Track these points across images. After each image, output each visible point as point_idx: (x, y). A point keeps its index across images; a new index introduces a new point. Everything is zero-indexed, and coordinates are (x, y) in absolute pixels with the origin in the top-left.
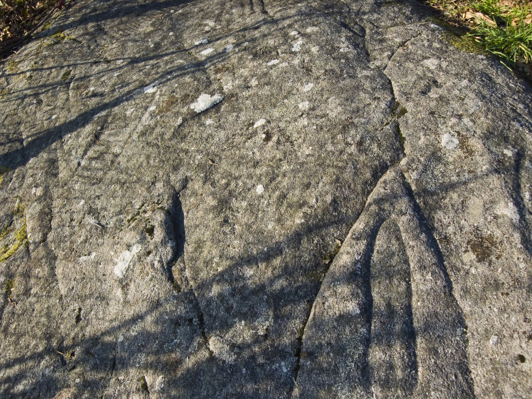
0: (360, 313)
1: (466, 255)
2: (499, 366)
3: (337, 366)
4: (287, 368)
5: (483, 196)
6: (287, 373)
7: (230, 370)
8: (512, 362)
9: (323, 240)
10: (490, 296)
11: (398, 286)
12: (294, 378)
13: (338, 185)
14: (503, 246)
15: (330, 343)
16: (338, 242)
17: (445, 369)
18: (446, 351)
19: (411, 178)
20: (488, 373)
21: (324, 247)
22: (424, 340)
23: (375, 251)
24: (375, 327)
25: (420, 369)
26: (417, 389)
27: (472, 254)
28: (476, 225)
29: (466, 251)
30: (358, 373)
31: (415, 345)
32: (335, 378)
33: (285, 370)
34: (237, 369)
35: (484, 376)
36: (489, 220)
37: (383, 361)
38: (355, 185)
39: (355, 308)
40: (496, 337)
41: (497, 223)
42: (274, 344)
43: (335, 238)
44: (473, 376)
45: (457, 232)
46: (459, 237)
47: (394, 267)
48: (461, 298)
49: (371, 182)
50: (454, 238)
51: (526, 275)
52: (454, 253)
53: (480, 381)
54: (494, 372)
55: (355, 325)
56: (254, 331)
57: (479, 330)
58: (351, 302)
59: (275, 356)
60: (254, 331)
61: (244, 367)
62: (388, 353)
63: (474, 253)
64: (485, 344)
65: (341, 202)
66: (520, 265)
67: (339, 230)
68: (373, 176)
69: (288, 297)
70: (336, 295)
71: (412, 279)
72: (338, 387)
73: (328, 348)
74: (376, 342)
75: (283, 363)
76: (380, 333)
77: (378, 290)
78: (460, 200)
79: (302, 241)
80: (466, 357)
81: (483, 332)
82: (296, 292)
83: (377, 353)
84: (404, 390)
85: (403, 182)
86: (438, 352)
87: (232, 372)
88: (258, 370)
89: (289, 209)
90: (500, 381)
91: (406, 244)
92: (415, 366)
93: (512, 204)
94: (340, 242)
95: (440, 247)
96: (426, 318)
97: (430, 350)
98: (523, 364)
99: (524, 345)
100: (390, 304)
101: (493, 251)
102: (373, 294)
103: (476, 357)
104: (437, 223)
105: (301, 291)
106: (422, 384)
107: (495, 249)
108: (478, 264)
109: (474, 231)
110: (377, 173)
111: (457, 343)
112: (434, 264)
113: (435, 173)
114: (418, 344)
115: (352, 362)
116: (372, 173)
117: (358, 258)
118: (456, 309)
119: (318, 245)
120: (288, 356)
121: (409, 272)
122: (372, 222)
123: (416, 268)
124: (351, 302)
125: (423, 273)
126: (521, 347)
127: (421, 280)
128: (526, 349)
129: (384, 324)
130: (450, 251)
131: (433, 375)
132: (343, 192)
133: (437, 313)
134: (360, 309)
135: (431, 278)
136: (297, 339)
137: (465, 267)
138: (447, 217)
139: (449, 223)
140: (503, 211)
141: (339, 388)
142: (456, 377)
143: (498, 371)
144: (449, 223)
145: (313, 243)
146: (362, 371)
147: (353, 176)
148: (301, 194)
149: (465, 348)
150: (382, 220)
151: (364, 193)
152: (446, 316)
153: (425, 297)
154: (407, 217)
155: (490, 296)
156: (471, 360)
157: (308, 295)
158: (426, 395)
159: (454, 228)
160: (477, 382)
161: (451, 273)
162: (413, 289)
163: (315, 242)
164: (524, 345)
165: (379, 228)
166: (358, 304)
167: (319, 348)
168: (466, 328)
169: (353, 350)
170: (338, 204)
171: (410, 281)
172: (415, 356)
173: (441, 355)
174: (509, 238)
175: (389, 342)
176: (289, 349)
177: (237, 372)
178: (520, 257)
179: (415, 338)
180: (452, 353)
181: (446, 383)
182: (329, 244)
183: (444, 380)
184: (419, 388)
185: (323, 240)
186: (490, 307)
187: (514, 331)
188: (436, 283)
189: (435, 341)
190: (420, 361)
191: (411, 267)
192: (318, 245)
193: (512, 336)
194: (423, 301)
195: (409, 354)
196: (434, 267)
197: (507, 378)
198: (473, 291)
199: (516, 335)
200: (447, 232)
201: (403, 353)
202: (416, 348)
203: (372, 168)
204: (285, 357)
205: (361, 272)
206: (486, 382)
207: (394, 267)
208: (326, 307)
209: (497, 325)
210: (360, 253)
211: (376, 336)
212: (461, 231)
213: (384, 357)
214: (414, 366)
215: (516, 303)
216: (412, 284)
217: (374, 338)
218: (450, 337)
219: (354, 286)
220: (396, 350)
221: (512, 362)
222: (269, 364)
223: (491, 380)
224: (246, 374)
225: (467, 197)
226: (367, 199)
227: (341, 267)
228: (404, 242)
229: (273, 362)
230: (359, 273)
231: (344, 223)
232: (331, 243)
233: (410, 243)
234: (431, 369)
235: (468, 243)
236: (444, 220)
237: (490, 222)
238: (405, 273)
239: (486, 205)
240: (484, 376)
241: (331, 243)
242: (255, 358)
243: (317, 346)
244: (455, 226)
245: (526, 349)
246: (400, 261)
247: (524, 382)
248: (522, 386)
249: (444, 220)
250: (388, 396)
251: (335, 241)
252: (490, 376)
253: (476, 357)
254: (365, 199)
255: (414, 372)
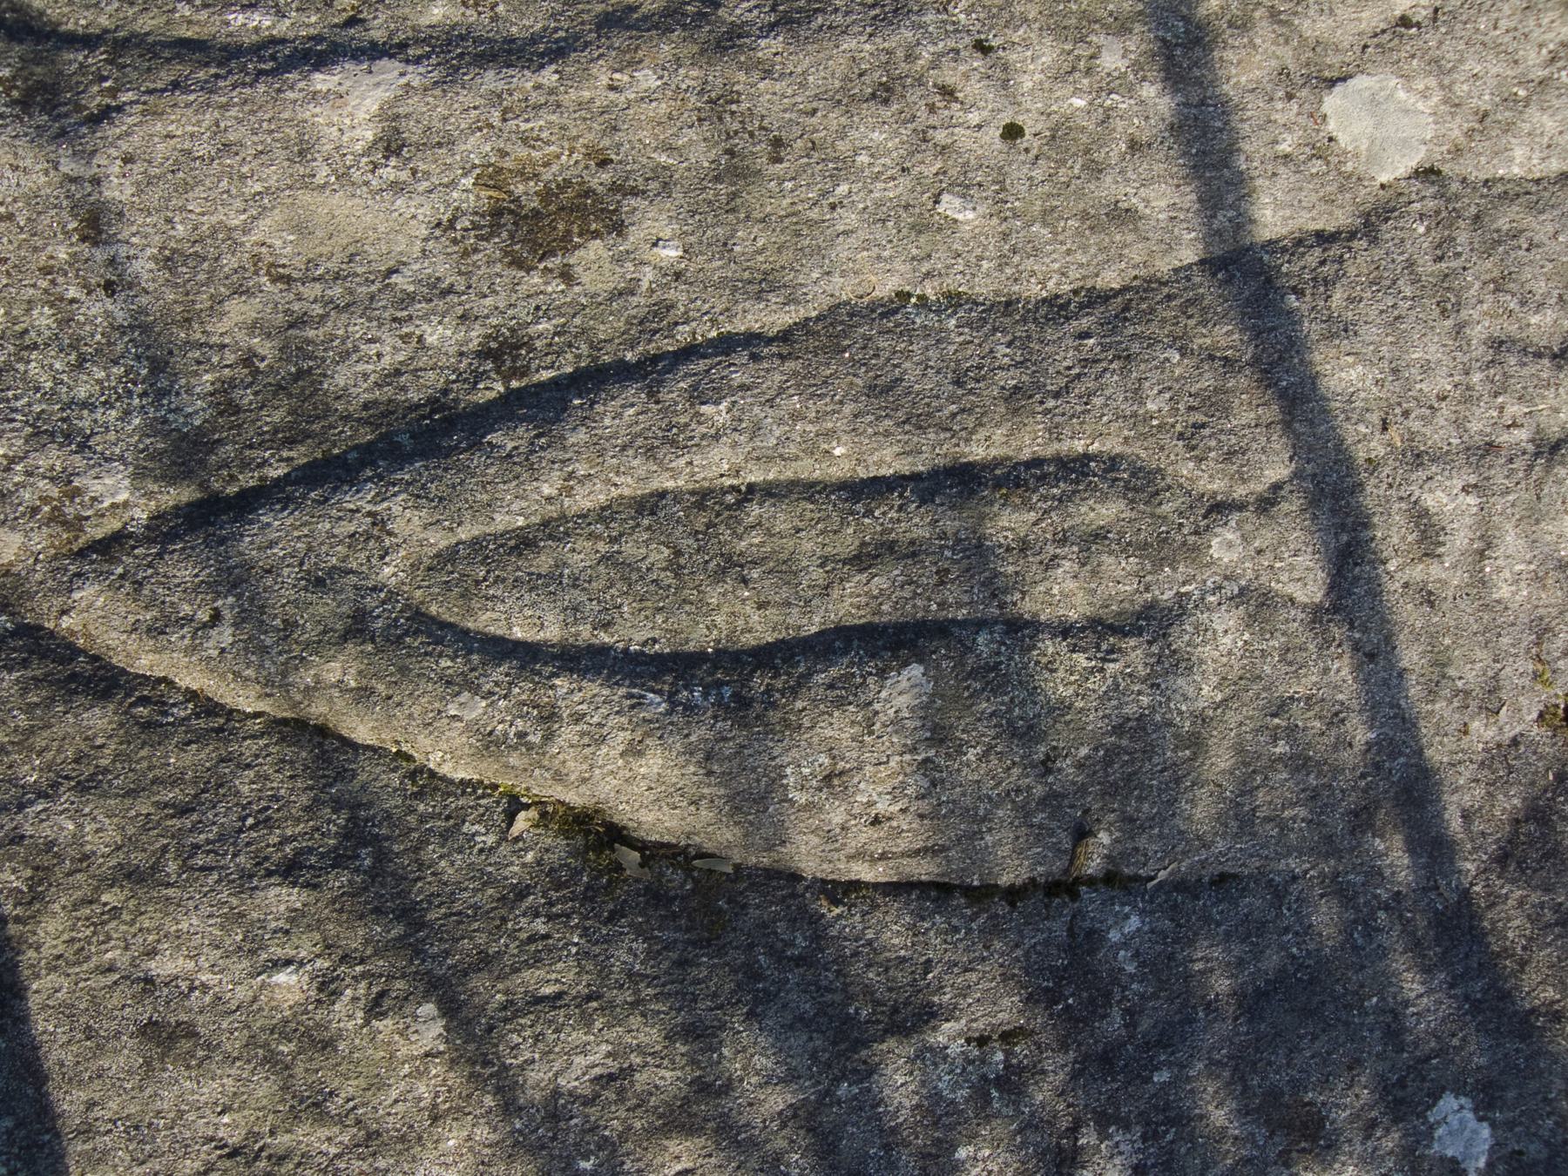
0: (920, 662)
1: (586, 278)
2: (1039, 203)
3: (1121, 726)
4: (1127, 917)
5: (258, 187)
6: (1142, 912)
7: (1166, 1132)
8: (1024, 163)
9: (522, 893)
10: (786, 202)
11: (769, 533)
12: (1150, 885)
13: (172, 867)
14: (544, 135)
15: (1043, 763)
16: (522, 822)
17: (1069, 368)
18: (1006, 360)
19: (126, 504)
20: (1060, 238)
21: (559, 886)
22: (982, 434)
23: (605, 638)
24: (960, 605)
25: (1079, 446)
26: (1143, 454)
27: (580, 253)
28: (425, 232)
29: (567, 275)
30: (1134, 649)
31: (998, 462)
32: (1158, 728)
33: (1134, 922)
34: (1156, 1107)
35: (1069, 252)
36: (404, 175)
37: (1084, 565)
38: (175, 781)
39: (904, 684)
40: (945, 198)
41: (420, 147)
42: (1047, 990)
43: (503, 838)
44: (1067, 288)
45: (459, 311)
46: (488, 301)
47: (678, 553)
48: (796, 302)
49: (144, 701)
50: (494, 321)
51: (694, 73)
52: (577, 321)
53: (1081, 265)
54: (1058, 220)
55: (969, 675)
56: (995, 1094)
57: (914, 251)
58: (877, 706)
59: (1094, 973)
60: (995, 1094)
61: (1149, 1080)
62: (1051, 550)
63: (577, 247)
64: (967, 236)
65: (285, 840)
66: (644, 86)
67: (457, 826)
68: (104, 695)
69: (828, 990)
70: (842, 773)
71: (728, 482)
72: (1180, 713)
73: (1060, 770)
74: (1017, 596)
75: (1114, 936)
76: (983, 584)
77: (795, 611)
78: (268, 287)
79: (548, 990)
80: (1008, 304)
81: (922, 239)
82: (799, 961)
83: (1055, 591)
84: (1157, 493)
85: (150, 541)
86: (1015, 387)
87: (1170, 1122)
88: (1145, 1024)
89: (331, 1107)
90: (1081, 206)
91: (552, 511)
92: (1074, 460)
93: (318, 76)
94: (522, 815)
95: (546, 375)
96: (898, 425)
97: (1016, 411)
98: (1027, 131)
99: (974, 118)
100: (856, 557)
101: (567, 174)
102: (814, 629)
103: (1009, 271)
104: (404, 389)
105: (792, 944)
106: (1126, 438)
107: (555, 168)
108: (635, 235)
109: (455, 242)
110: (74, 677)
111: (969, 324)
112: (651, 395)
113: (82, 392)
114: (994, 452)
115: (1102, 670)
116: (80, 700)
117: (657, 704)
118: (842, 323)
119: (557, 909)
120: (1087, 924)
121: (693, 493)
122: (445, 663)
123: (682, 462)
124: (877, 706)
125: (703, 437)
126: (979, 127)
127: (735, 445)
128: (985, 113)
129: (947, 571)
130: (567, 338)
131: (1098, 401)
132: (221, 838)
133: (872, 388)
134: (905, 664)
135: (723, 406)
136: (1013, 905)
137: (645, 285)
138: (373, 349)
139: (405, 338)
140: (361, 115)
141: (1184, 708)
142: (1085, 335)
143: (1053, 209)
144: (405, 338)
145: (547, 937)
146: (1125, 635)
147: (104, 795)
148: (230, 1060)
149: (976, 304)
150: (420, 621)
151: (221, 730)
152: (876, 356)
153: (809, 428)
154: (396, 510)
155: (786, 202)
156: (1016, 288)
157: (803, 909)
158: (1159, 426)
159: (435, 319)
160: (1084, 278)
161: (683, 334)
162: (771, 476)
163: (540, 926)
164: (974, 118)
165: (466, 632)
166: (882, 674)
167: (1060, 806)
168: (903, 296)
169: (1061, 674)
170: (299, 853)
171: (734, 489)
172: (1036, 462)
173: (1025, 378)
174: (505, 112)
175: (1009, 549)
176: (1055, 925)
177: (1167, 1103)
178: (604, 80)
179: (969, 464)
180: (1009, 345)
181: (1114, 366)
182: (539, 862)
183: (1105, 370)
184: (1137, 450)
185: (522, 893)
186: (833, 207)
187: (925, 140)
188: (743, 387)
189: (979, 395)
190: (1056, 446)
191: (670, 484)
192: (557, 909)
193: (943, 150)
194: (829, 434)
195: (1042, 478)
196: (667, 396)
197: (1073, 187)
198: (761, 258)
199: (940, 136)
200: (452, 350)
201: (1044, 498)
202: (1009, 458)
203: (49, 703)
204: (1090, 933)
205: (719, 684)
206: (1084, 248)
207: (678, 553)
208: (895, 808)
209: (899, 189)
210: (630, 696)
211: (994, 596)
212: (450, 290)
213: (1067, 564)
214: (1075, 469)
215: (814, 120)
216: (752, 478)
217: (1002, 606)
218: (952, 348)
219: (799, 705)
220: (1035, 524)
221: (1024, 163)
222: (1125, 988)
223: (1079, 233)
224: (1169, 1064)
225: (256, 258)
226: (257, 715)
227: (710, 773)
228: (535, 519)
229: (1116, 974)
230: (727, 692)
231: (413, 811)
232: (530, 857)
233: (547, 490)
234: (1079, 408)
235: (518, 263)
236: (386, 360)
237: (414, 172)
238: (700, 506)
239: (319, 180)
240: (1069, 252)
241: (530, 857)
242: (1105, 1052)
243: (1051, 817)
244: (425, 317)
245: (985, 113)
246: (649, 528)
247: (1084, 139)
248: (1094, 147)
249: (386, 360)
250: (1184, 543)
251: (517, 839)
252: (1068, 233)
253: (1009, 271)
254: (256, 725)
255: (1093, 464)
